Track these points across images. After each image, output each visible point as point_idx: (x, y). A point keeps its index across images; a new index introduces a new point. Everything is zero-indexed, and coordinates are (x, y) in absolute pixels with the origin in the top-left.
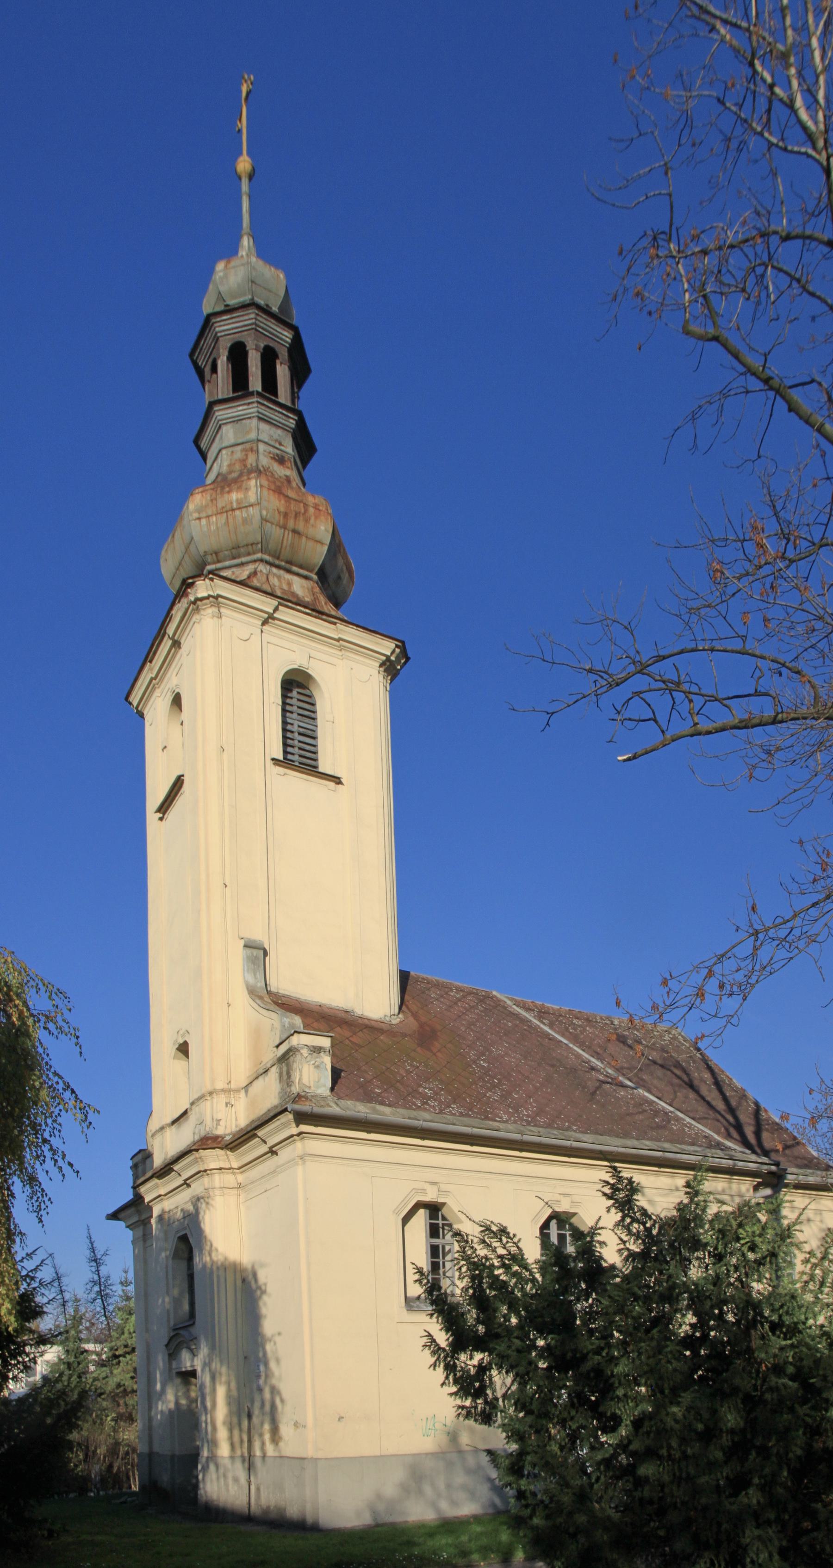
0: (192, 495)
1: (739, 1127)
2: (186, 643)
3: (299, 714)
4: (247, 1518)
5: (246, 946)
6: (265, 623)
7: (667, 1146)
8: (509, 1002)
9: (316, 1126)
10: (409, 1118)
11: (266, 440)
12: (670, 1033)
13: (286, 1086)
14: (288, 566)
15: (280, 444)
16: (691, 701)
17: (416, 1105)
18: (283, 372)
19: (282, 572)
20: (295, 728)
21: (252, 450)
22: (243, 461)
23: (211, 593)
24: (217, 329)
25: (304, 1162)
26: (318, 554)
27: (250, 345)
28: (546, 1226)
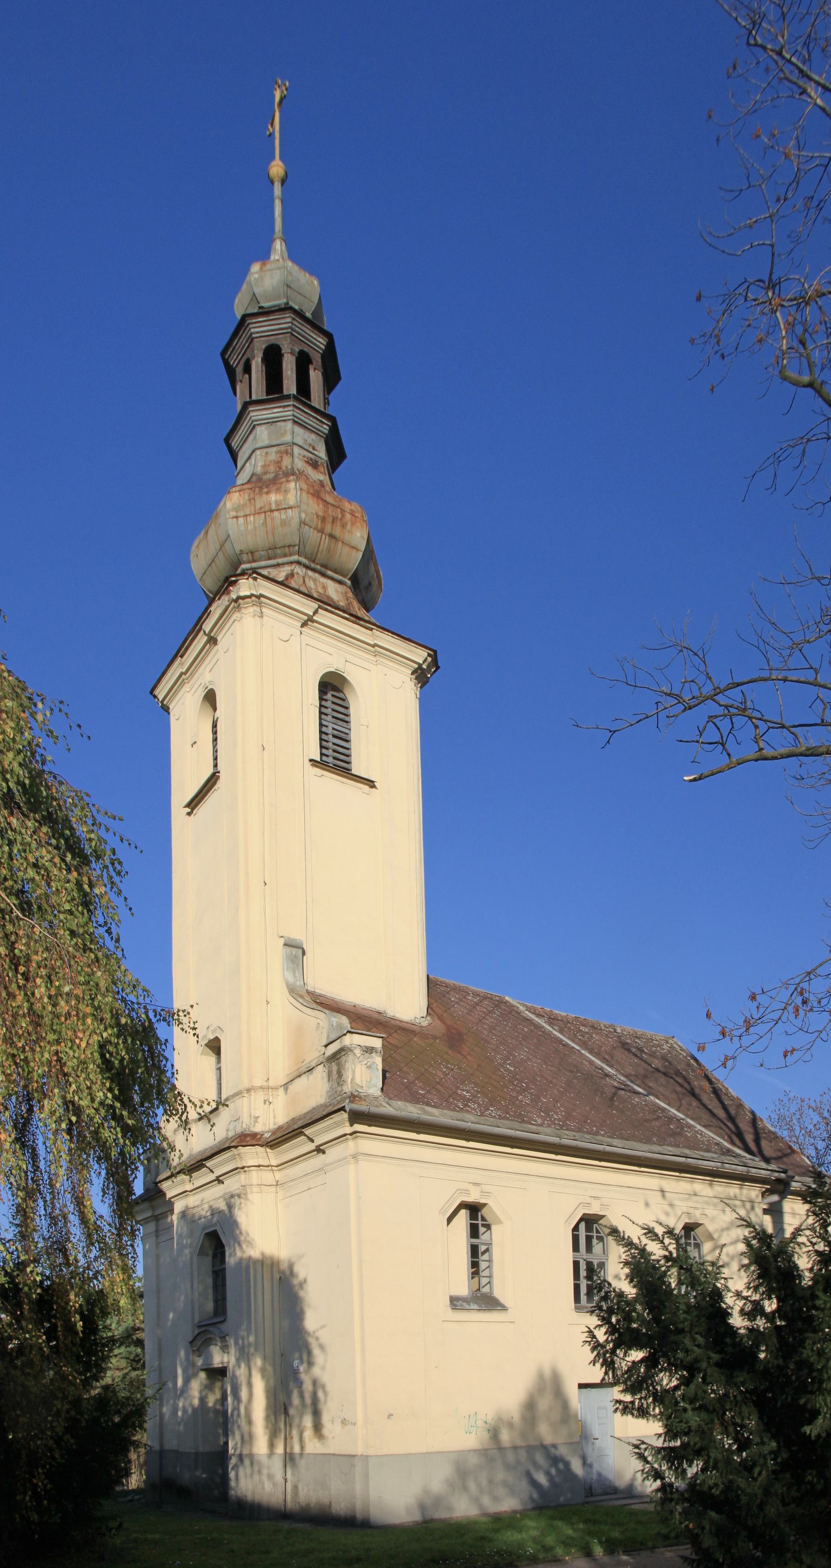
0: (229, 493)
1: (740, 1134)
2: (224, 640)
3: (333, 717)
4: (282, 1515)
5: (285, 945)
6: (304, 625)
7: (687, 1152)
8: (522, 1008)
9: (370, 1125)
10: (458, 1120)
11: (301, 444)
12: (667, 1042)
13: (336, 1085)
14: (323, 570)
15: (314, 449)
16: (756, 727)
17: (459, 1107)
18: (316, 377)
19: (317, 575)
20: (329, 730)
21: (286, 452)
22: (278, 463)
23: (255, 593)
24: (252, 330)
25: (357, 1161)
26: (353, 560)
27: (286, 348)
28: (576, 1228)
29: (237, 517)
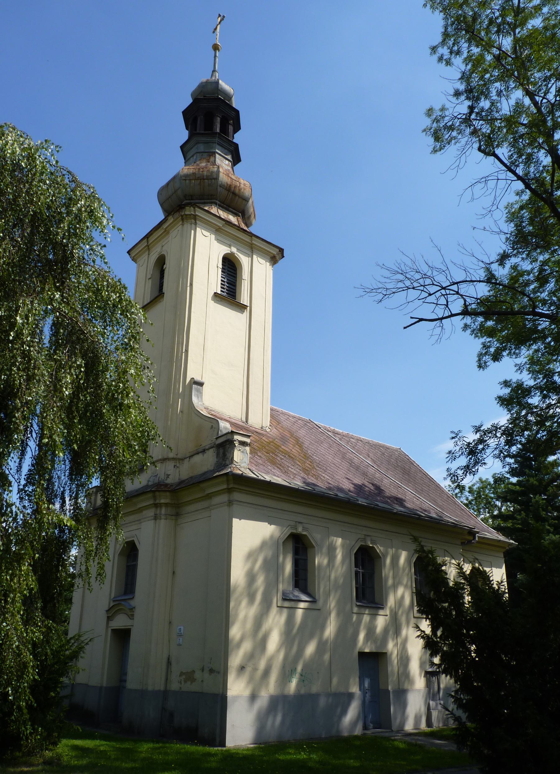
29: (185, 180)
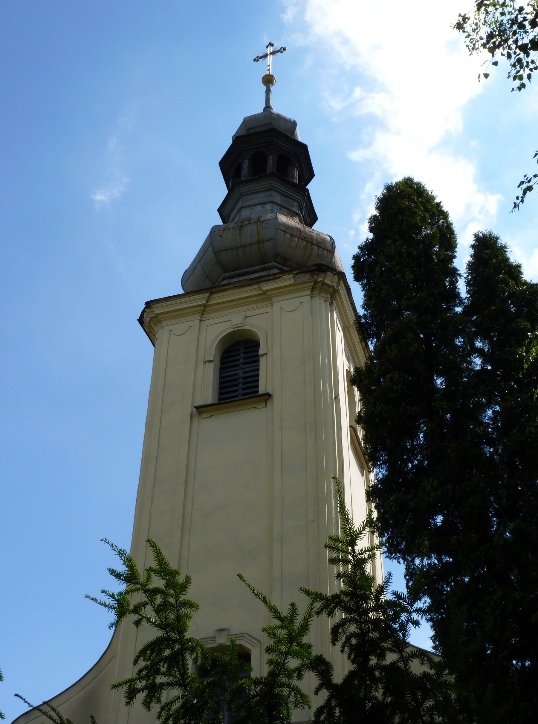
29: (285, 232)
